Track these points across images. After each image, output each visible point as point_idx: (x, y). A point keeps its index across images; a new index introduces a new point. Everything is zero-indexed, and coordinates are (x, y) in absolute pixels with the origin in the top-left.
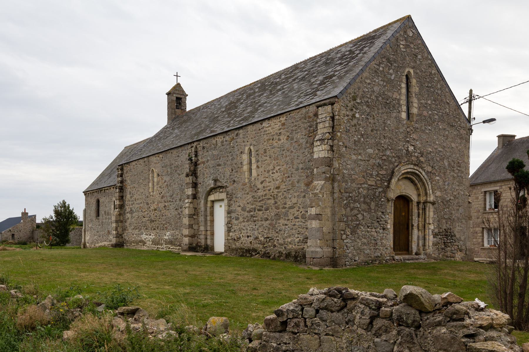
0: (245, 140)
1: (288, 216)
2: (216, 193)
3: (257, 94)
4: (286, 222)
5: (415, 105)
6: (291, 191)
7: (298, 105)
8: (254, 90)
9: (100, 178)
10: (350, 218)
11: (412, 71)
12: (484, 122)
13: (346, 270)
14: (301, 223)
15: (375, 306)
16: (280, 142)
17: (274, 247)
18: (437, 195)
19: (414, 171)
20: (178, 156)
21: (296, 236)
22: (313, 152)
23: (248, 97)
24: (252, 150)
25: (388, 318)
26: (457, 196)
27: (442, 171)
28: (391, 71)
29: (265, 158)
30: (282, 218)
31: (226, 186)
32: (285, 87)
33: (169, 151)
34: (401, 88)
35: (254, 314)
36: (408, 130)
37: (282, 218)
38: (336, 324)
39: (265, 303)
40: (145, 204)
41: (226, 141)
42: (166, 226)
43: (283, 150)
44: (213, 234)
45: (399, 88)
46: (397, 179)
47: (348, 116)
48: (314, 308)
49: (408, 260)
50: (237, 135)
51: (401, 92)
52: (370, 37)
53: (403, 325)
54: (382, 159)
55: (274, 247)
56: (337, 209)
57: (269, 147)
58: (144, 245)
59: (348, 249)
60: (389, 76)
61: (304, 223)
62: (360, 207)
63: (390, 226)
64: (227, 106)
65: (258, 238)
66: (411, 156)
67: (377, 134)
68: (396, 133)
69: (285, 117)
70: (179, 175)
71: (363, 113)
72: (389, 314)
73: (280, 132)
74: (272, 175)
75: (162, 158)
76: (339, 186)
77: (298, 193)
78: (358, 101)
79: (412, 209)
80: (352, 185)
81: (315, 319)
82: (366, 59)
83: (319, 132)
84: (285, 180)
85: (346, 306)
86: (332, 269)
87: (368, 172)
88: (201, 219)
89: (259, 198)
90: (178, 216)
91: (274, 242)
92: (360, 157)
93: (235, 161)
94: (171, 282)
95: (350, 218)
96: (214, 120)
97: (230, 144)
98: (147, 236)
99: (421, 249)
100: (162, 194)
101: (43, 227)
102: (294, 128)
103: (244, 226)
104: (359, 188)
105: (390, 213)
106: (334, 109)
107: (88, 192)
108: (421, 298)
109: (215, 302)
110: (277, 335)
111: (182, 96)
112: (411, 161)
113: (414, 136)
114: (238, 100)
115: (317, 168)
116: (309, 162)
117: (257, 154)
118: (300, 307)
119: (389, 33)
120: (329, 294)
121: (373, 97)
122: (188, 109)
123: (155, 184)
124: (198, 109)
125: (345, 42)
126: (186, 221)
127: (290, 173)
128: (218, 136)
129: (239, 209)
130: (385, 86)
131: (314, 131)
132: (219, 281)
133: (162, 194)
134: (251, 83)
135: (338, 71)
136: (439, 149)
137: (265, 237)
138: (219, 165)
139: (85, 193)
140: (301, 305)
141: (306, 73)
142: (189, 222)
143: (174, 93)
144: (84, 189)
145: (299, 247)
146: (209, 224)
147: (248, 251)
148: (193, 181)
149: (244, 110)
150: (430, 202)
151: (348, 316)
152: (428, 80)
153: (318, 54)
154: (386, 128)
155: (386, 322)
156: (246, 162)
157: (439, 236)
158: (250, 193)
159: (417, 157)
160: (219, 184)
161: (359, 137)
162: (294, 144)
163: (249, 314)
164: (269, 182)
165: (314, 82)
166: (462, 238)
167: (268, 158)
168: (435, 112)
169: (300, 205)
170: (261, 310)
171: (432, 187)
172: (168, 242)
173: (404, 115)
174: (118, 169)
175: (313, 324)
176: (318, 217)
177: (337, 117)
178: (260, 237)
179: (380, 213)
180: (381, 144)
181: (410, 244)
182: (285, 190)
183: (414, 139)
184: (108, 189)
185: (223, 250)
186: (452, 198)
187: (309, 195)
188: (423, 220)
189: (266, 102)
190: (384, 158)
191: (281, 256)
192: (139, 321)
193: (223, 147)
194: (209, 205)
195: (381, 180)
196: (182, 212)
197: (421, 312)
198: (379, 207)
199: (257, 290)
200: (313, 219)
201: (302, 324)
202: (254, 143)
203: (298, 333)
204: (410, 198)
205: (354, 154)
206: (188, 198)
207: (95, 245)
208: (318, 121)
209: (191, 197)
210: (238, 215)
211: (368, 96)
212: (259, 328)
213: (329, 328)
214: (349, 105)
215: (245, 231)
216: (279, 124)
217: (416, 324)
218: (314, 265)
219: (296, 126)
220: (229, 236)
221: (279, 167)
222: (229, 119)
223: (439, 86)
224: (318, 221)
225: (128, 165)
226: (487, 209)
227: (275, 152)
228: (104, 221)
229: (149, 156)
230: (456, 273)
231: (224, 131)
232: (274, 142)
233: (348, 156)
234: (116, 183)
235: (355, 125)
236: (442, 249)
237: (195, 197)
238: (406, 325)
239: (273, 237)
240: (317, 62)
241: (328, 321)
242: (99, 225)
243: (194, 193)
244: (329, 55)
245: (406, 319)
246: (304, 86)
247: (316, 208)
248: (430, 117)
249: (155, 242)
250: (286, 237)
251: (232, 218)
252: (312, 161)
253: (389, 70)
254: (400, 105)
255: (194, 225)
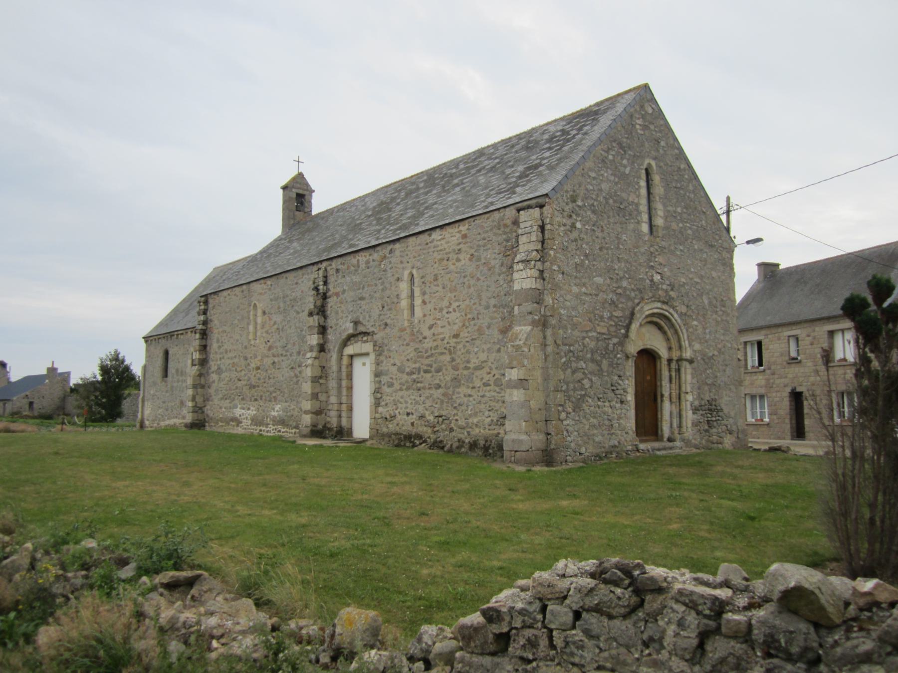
0: (405, 259)
1: (472, 382)
2: (356, 342)
3: (422, 191)
4: (469, 391)
5: (660, 213)
6: (478, 342)
7: (487, 207)
8: (417, 185)
9: (171, 317)
10: (571, 386)
11: (653, 163)
12: (748, 242)
13: (570, 471)
14: (494, 394)
15: (711, 609)
16: (458, 264)
17: (450, 432)
18: (695, 348)
19: (662, 311)
20: (297, 283)
21: (487, 413)
22: (512, 280)
23: (407, 195)
24: (415, 276)
25: (740, 637)
26: (723, 350)
27: (701, 313)
28: (625, 162)
29: (436, 288)
30: (464, 384)
31: (373, 332)
32: (465, 181)
33: (283, 275)
34: (640, 187)
35: (425, 572)
36: (652, 249)
37: (464, 384)
38: (621, 645)
39: (444, 545)
40: (242, 358)
41: (373, 261)
42: (274, 395)
43: (464, 277)
44: (350, 409)
45: (637, 187)
46: (638, 324)
47: (564, 225)
48: (571, 608)
49: (659, 450)
50: (391, 251)
51: (639, 193)
52: (591, 111)
53: (777, 657)
54: (617, 294)
55: (450, 432)
56: (551, 372)
57: (442, 272)
58: (238, 426)
59: (569, 436)
60: (622, 169)
61: (498, 393)
62: (586, 369)
63: (630, 397)
64: (374, 208)
65: (425, 417)
66: (658, 289)
67: (608, 254)
68: (635, 253)
69: (467, 225)
70: (298, 313)
71: (587, 223)
72: (743, 628)
73: (459, 248)
74: (447, 316)
75: (271, 285)
76: (553, 334)
77: (489, 346)
78: (580, 203)
79: (661, 370)
80: (574, 333)
81: (574, 632)
82: (588, 142)
83: (522, 248)
84: (467, 324)
85: (641, 604)
86: (546, 469)
87: (597, 312)
88: (333, 384)
89: (426, 352)
90: (295, 380)
91: (450, 423)
92: (584, 290)
93: (388, 292)
94: (276, 500)
95: (571, 386)
96: (356, 228)
97: (380, 265)
98: (243, 411)
99: (676, 432)
100: (269, 344)
101: (81, 390)
102: (481, 243)
103: (402, 397)
104: (584, 338)
105: (630, 376)
106: (544, 215)
107: (151, 338)
108: (820, 595)
109: (353, 545)
110: (487, 661)
111: (305, 193)
112: (658, 296)
113: (660, 259)
114: (393, 199)
115: (519, 305)
116: (505, 295)
117: (423, 283)
118: (537, 605)
119: (620, 108)
120: (604, 579)
121: (601, 199)
122: (314, 213)
123: (259, 327)
124: (330, 212)
125: (553, 119)
126: (307, 387)
127: (476, 312)
128: (361, 253)
129: (394, 369)
130: (616, 184)
131: (513, 248)
132: (360, 497)
133: (269, 344)
134: (413, 174)
135: (547, 158)
136: (695, 280)
137: (436, 414)
138: (362, 299)
139: (147, 339)
140: (540, 599)
141: (497, 160)
142: (312, 390)
143: (293, 187)
144: (145, 333)
145: (491, 432)
146: (344, 392)
147: (408, 437)
148: (319, 324)
149: (402, 215)
150: (686, 360)
151: (648, 629)
152: (676, 178)
153: (514, 134)
154: (621, 247)
155: (738, 647)
156: (405, 294)
157: (701, 412)
158: (411, 344)
159: (666, 291)
160: (361, 329)
161: (582, 258)
162: (481, 268)
163: (416, 572)
164: (442, 327)
165: (510, 174)
166: (732, 414)
167: (440, 288)
168: (688, 225)
169: (492, 363)
170: (438, 561)
171: (688, 336)
172: (278, 421)
173: (645, 228)
174: (199, 302)
175: (567, 644)
176: (522, 383)
177: (548, 227)
178: (427, 415)
179: (616, 378)
180: (615, 269)
181: (659, 423)
182: (467, 339)
183: (661, 264)
184: (182, 334)
185: (366, 436)
186: (716, 353)
187: (508, 348)
188: (677, 387)
189: (436, 203)
190: (619, 291)
191: (462, 446)
192: (200, 601)
193: (369, 270)
194: (345, 361)
195: (616, 325)
196: (300, 372)
197: (817, 626)
198: (614, 368)
199: (427, 515)
200: (515, 387)
201: (544, 642)
202: (419, 264)
203: (534, 660)
204: (657, 354)
205: (575, 285)
206: (311, 351)
207: (158, 424)
208: (520, 232)
209: (316, 349)
210: (392, 378)
211: (594, 197)
212: (445, 637)
213: (606, 654)
214: (567, 208)
215: (404, 405)
216: (458, 235)
217: (810, 655)
218: (517, 462)
219: (484, 239)
220: (376, 412)
221: (457, 304)
222: (378, 227)
223: (691, 188)
224: (522, 391)
225: (216, 296)
226: (749, 367)
227: (452, 279)
228: (175, 384)
229: (249, 283)
230: (736, 471)
231: (371, 244)
232: (450, 263)
233: (566, 287)
234: (195, 324)
235: (576, 240)
236: (706, 431)
237: (322, 348)
238: (784, 656)
239: (449, 416)
240: (513, 146)
241: (602, 639)
242: (167, 392)
243: (322, 342)
244: (531, 136)
245: (786, 643)
246: (495, 180)
247: (518, 369)
248: (681, 232)
249: (256, 421)
250: (470, 416)
251: (383, 383)
252: (510, 294)
253: (622, 159)
254: (639, 213)
255: (319, 395)
